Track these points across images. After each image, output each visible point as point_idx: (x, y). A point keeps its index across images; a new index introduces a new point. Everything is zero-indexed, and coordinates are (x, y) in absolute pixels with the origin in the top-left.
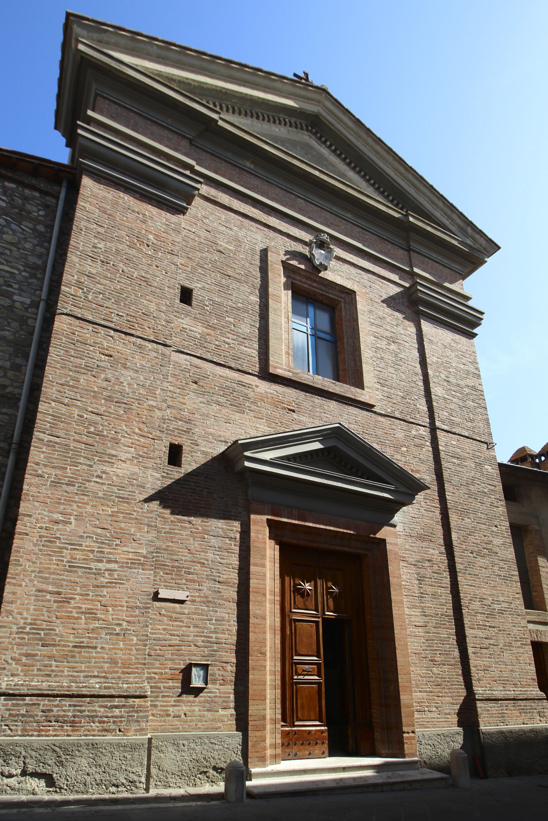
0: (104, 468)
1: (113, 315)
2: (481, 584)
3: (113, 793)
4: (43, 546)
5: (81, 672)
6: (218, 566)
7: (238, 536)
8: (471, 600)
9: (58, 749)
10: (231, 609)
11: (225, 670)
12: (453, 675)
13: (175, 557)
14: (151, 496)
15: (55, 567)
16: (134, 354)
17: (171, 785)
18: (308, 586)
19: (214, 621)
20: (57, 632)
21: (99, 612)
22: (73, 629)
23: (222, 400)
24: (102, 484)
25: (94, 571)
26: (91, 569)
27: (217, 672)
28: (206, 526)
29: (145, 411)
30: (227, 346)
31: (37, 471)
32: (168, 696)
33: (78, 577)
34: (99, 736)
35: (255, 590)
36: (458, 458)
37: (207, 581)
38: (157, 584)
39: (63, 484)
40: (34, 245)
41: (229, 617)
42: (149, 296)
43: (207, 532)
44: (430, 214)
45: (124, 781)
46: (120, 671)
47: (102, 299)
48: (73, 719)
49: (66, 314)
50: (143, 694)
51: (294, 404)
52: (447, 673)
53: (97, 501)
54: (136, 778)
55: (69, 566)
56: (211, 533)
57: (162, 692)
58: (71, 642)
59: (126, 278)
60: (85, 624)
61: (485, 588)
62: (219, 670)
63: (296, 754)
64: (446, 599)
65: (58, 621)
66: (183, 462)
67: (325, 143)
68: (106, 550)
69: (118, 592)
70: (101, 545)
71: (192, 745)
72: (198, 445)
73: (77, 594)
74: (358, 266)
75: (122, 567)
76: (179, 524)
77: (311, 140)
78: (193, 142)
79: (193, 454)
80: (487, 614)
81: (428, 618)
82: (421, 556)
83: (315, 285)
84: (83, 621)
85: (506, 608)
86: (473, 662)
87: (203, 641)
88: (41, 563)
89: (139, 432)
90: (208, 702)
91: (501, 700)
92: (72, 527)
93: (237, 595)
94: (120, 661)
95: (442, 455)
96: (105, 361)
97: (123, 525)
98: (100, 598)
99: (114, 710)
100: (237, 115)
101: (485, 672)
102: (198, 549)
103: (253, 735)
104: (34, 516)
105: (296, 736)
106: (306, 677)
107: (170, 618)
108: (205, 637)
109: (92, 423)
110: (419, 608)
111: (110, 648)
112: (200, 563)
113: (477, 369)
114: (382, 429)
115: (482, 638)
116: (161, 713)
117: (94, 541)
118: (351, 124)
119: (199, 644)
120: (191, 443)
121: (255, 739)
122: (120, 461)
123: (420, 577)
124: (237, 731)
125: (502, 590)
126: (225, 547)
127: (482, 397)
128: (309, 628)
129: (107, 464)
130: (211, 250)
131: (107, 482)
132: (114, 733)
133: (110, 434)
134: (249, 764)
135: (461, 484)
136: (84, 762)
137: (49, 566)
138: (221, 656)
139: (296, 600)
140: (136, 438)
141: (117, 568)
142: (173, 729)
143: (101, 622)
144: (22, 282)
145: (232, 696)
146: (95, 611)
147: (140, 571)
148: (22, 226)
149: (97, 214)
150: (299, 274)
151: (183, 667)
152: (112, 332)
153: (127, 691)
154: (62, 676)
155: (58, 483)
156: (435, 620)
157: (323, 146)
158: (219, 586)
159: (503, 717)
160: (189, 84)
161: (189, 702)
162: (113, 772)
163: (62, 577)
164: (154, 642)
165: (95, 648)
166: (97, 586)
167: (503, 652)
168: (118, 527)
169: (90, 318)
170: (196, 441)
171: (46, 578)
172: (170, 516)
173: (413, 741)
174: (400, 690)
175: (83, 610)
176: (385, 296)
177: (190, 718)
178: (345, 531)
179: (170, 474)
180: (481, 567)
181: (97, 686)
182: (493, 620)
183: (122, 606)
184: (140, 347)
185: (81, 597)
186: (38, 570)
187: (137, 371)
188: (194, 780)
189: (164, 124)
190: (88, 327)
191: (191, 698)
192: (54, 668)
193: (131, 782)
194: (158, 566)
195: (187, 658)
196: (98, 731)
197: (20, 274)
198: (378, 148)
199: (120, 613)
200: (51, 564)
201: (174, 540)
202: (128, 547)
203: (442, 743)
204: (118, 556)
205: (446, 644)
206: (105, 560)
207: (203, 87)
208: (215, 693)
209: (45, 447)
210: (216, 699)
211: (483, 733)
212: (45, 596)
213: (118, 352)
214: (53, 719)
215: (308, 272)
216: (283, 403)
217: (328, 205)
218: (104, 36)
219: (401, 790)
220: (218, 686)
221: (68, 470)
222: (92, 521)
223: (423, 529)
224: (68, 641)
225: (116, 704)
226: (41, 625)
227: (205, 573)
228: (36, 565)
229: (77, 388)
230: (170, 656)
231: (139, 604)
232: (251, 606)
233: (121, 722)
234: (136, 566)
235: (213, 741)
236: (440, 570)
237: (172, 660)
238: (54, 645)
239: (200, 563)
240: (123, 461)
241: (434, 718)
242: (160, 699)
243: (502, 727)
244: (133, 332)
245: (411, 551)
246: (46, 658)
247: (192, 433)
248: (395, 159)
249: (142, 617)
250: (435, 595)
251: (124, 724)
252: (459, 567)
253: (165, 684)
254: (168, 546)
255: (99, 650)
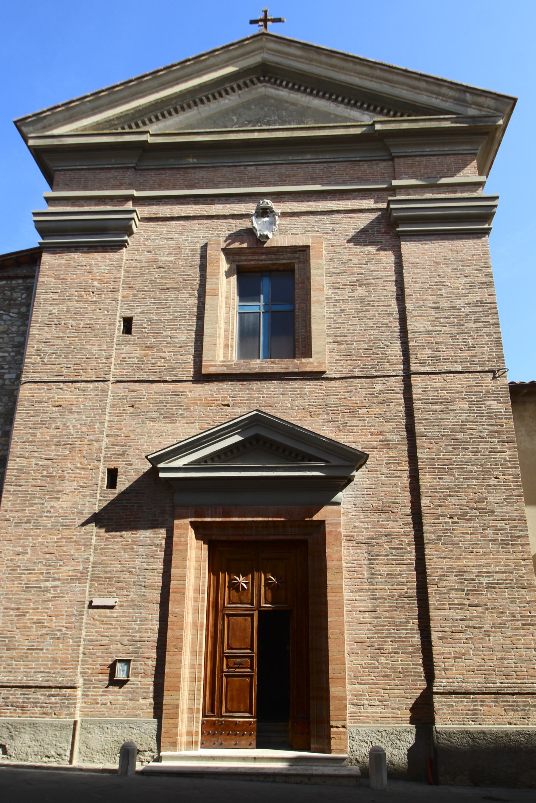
0: (53, 503)
1: (63, 369)
2: (461, 555)
3: (45, 762)
4: (9, 574)
5: (32, 668)
6: (145, 572)
7: (163, 542)
8: (444, 575)
9: (10, 727)
10: (154, 610)
11: (146, 664)
12: (408, 665)
13: (107, 569)
14: (88, 519)
15: (17, 589)
16: (78, 398)
17: (95, 761)
18: (241, 580)
19: (138, 622)
20: (17, 639)
21: (46, 621)
22: (28, 636)
23: (155, 415)
24: (51, 517)
25: (43, 589)
26: (40, 587)
27: (139, 666)
28: (136, 537)
29: (86, 446)
30: (163, 360)
31: (5, 516)
32: (97, 687)
33: (32, 595)
34: (40, 718)
35: (175, 590)
36: (441, 403)
37: (134, 587)
38: (92, 594)
39: (22, 523)
40: (19, 326)
41: (152, 617)
42: (92, 340)
43: (135, 543)
44: (413, 103)
45: (54, 754)
46: (60, 667)
47: (55, 358)
48: (22, 704)
49: (29, 382)
50: (72, 685)
51: (229, 398)
52: (400, 662)
53: (46, 532)
54: (62, 752)
55: (26, 587)
56: (139, 543)
57: (93, 684)
58: (26, 646)
59: (74, 331)
60: (36, 631)
61: (468, 558)
62: (141, 664)
63: (221, 744)
64: (408, 578)
65: (18, 631)
66: (117, 484)
67: (281, 85)
68: (52, 571)
69: (60, 604)
70: (49, 568)
71: (114, 729)
72: (131, 465)
73: (30, 609)
74: (318, 212)
75: (64, 583)
76: (112, 540)
77: (268, 89)
78: (137, 168)
79: (127, 473)
80: (468, 590)
81: (378, 601)
82: (376, 531)
83: (263, 257)
84: (34, 629)
85: (502, 580)
86: (437, 647)
87: (128, 640)
88: (7, 587)
89: (81, 466)
90: (130, 692)
91: (474, 694)
92: (29, 556)
93: (161, 597)
94: (60, 660)
95: (417, 404)
96: (55, 412)
97: (65, 549)
98: (46, 610)
99: (51, 697)
100: (182, 112)
101: (457, 660)
102: (127, 560)
103: (166, 722)
104: (3, 552)
105: (222, 726)
106: (238, 670)
107: (102, 622)
108: (130, 636)
109: (45, 468)
110: (368, 592)
111: (52, 650)
112: (129, 572)
113: (490, 275)
114: (334, 395)
115: (456, 620)
116: (92, 701)
117: (44, 565)
118: (298, 52)
119: (124, 643)
120: (126, 464)
121: (168, 726)
122: (65, 495)
123: (372, 556)
124: (154, 718)
125: (497, 558)
126: (151, 554)
127: (494, 311)
128: (244, 622)
129: (55, 500)
130: (152, 270)
131: (54, 515)
132: (50, 716)
133: (58, 473)
134: (162, 748)
135: (442, 435)
136: (27, 737)
137: (12, 589)
138: (143, 652)
139: (231, 595)
140: (78, 471)
141: (59, 585)
142: (100, 715)
143: (47, 629)
144: (11, 361)
145: (152, 688)
146: (43, 621)
147: (77, 585)
148: (11, 314)
149: (53, 283)
150: (243, 253)
151: (111, 662)
152: (62, 384)
153: (61, 683)
154: (19, 672)
155: (20, 523)
156: (389, 603)
157: (281, 88)
158: (144, 590)
159: (475, 714)
160: (127, 115)
161: (114, 692)
162: (46, 746)
163: (21, 596)
164: (88, 642)
165: (42, 649)
166: (45, 601)
167: (489, 635)
168: (61, 551)
169: (46, 378)
170: (130, 461)
171: (10, 599)
172: (105, 534)
173: (343, 737)
174: (330, 681)
175: (35, 620)
176: (352, 233)
177: (114, 706)
178: (275, 519)
179: (107, 497)
180: (463, 533)
181: (41, 679)
182: (476, 596)
183: (63, 615)
184: (84, 390)
185: (33, 611)
186: (5, 593)
187: (80, 412)
188: (115, 758)
189: (110, 166)
190: (43, 387)
191: (116, 689)
192: (14, 666)
193: (59, 755)
194: (95, 578)
195: (114, 655)
196: (40, 714)
197: (9, 355)
198: (334, 61)
199: (61, 620)
200: (13, 587)
201: (107, 554)
202: (68, 566)
203: (383, 741)
204: (61, 575)
205: (403, 629)
206: (51, 579)
207: (139, 110)
208: (137, 684)
209: (11, 496)
210: (138, 690)
211: (437, 732)
212: (9, 612)
213: (66, 401)
214: (10, 704)
215: (251, 248)
216: (217, 400)
217: (282, 158)
218: (46, 122)
219: (297, 783)
220: (140, 679)
221: (27, 511)
222: (43, 549)
223: (382, 500)
224: (24, 645)
225: (52, 693)
226: (6, 634)
227: (133, 580)
228: (4, 589)
229: (35, 442)
230: (100, 654)
231: (75, 613)
232: (170, 606)
233: (56, 707)
234: (74, 581)
235: (132, 726)
236: (402, 545)
237: (102, 657)
238: (14, 649)
239: (129, 572)
240: (67, 494)
241: (377, 713)
242: (91, 690)
243: (472, 727)
244: (79, 378)
245: (362, 528)
246: (9, 659)
247: (127, 454)
248: (355, 63)
249: (77, 622)
250: (391, 574)
251: (58, 709)
252: (427, 537)
253: (96, 678)
254: (102, 561)
255: (45, 651)
